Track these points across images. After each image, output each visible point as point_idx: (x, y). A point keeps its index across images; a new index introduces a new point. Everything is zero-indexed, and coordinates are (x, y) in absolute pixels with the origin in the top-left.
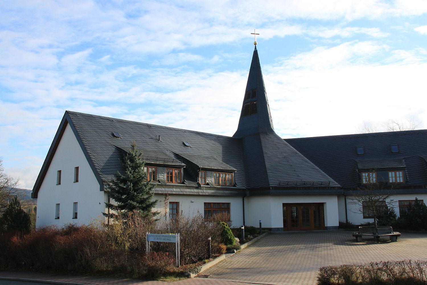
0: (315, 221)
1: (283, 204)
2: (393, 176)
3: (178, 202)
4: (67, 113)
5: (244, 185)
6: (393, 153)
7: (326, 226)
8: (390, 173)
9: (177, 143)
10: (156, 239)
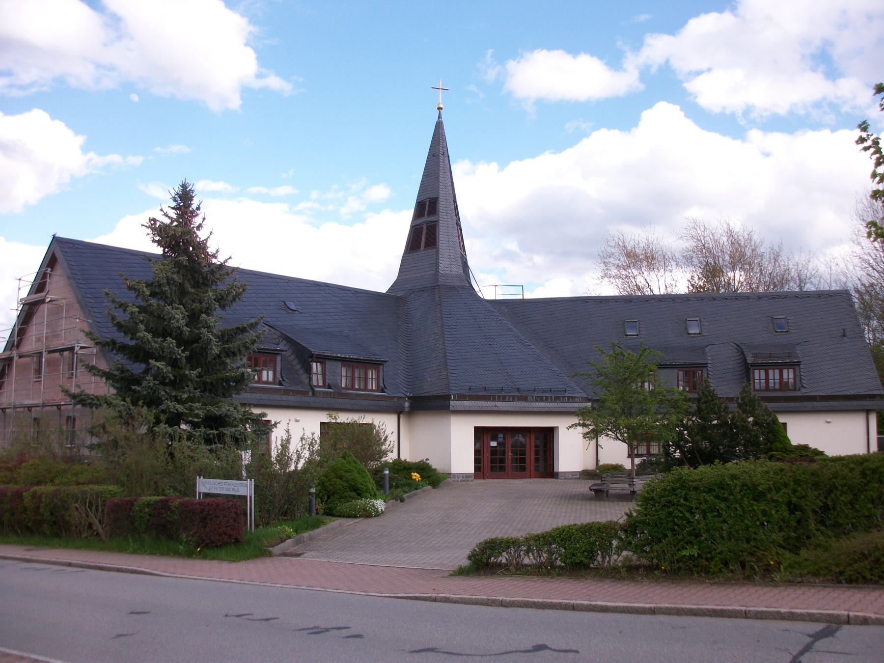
0: (537, 460)
1: (475, 428)
2: (761, 378)
3: (786, 423)
4: (57, 242)
5: (400, 389)
6: (692, 334)
7: (555, 471)
8: (756, 372)
9: (272, 304)
10: (213, 488)
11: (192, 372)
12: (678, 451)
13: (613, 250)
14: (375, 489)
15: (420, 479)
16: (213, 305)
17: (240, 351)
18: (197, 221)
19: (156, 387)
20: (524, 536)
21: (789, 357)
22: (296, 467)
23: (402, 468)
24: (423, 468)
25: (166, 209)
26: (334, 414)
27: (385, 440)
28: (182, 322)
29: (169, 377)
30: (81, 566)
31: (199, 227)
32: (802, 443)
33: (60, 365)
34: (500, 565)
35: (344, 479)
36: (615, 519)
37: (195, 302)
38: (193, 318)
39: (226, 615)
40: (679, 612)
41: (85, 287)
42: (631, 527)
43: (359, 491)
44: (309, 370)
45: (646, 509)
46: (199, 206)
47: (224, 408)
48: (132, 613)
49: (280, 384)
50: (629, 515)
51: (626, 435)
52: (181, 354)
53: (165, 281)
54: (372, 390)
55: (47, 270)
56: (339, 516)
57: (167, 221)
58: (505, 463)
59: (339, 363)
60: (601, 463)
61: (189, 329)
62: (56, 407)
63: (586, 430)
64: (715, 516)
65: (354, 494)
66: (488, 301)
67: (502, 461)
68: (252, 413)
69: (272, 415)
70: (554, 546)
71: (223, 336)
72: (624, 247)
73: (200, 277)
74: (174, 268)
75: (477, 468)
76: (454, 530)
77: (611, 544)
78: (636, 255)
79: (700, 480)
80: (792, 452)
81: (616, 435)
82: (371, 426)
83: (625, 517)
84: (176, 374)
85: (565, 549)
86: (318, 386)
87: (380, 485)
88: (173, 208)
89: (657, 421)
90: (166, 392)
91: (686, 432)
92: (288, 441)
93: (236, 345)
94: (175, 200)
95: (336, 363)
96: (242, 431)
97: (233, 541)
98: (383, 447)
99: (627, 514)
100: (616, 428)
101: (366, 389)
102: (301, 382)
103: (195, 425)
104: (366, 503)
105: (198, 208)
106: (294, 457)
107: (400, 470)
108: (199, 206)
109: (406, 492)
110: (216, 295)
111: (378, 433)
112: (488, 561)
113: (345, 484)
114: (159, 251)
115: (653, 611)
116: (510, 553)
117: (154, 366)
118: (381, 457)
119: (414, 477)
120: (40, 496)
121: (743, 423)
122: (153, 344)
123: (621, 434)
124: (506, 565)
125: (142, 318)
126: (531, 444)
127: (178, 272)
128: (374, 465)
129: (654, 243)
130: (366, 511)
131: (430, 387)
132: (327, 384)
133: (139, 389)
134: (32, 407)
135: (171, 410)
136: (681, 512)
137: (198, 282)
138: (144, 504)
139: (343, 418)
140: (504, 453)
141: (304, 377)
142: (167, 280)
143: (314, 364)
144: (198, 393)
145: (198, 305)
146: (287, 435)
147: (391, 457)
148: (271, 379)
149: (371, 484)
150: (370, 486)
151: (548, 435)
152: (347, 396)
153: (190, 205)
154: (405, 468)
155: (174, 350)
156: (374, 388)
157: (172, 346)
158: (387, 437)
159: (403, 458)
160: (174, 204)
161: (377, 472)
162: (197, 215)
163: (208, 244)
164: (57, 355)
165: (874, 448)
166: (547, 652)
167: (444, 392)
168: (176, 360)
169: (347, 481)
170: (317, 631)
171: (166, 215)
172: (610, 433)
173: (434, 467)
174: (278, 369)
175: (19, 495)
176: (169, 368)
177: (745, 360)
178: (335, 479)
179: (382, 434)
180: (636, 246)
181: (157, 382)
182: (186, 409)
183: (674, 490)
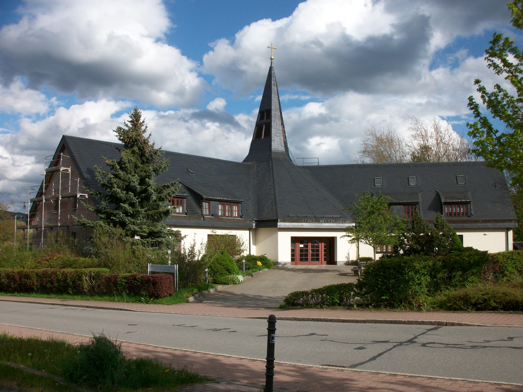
11: (142, 209)
12: (402, 250)
13: (369, 137)
14: (238, 270)
15: (261, 265)
16: (152, 174)
17: (166, 197)
18: (143, 128)
19: (124, 218)
20: (310, 290)
21: (465, 199)
22: (198, 258)
23: (251, 259)
24: (263, 259)
25: (127, 123)
26: (214, 230)
27: (243, 244)
28: (136, 183)
29: (130, 212)
30: (94, 308)
31: (144, 131)
32: (469, 246)
33: (68, 204)
34: (299, 305)
35: (222, 264)
36: (352, 282)
37: (142, 172)
38: (142, 181)
39: (173, 325)
40: (376, 322)
41: (81, 163)
42: (360, 285)
43: (230, 271)
44: (201, 207)
45: (366, 277)
46: (144, 121)
47: (158, 227)
48: (129, 325)
49: (186, 214)
50: (359, 280)
51: (371, 241)
52: (136, 200)
53: (127, 161)
54: (235, 217)
55: (61, 154)
56: (220, 284)
57: (127, 129)
58: (308, 257)
59: (218, 202)
60: (360, 257)
61: (140, 187)
62: (66, 227)
63: (350, 239)
64: (397, 281)
65: (227, 272)
66: (299, 167)
67: (306, 255)
68: (173, 230)
69: (184, 231)
70: (324, 295)
71: (157, 190)
72: (375, 135)
73: (145, 158)
74: (132, 154)
75: (293, 260)
76: (279, 290)
77: (350, 294)
78: (382, 140)
79: (390, 264)
80: (463, 251)
81: (366, 241)
82: (234, 236)
83: (357, 281)
84: (134, 211)
85: (329, 296)
86: (206, 215)
87: (241, 268)
88: (130, 122)
89: (388, 234)
90: (129, 220)
91: (406, 240)
92: (194, 245)
93: (164, 195)
94: (131, 118)
95: (216, 202)
96: (168, 240)
97: (169, 295)
98: (242, 248)
99: (358, 280)
100: (366, 237)
101: (232, 216)
102: (197, 213)
103: (142, 237)
104: (233, 277)
105: (143, 122)
106: (198, 253)
107: (251, 260)
108: (144, 121)
109: (254, 272)
110: (154, 169)
111: (239, 240)
112: (293, 302)
113: (222, 267)
114: (120, 142)
115: (364, 322)
116: (304, 298)
117: (123, 207)
118: (240, 253)
119: (258, 264)
120: (67, 274)
121: (436, 235)
122: (121, 194)
123: (369, 241)
124: (302, 304)
125: (115, 181)
126: (322, 246)
127: (133, 156)
128: (237, 257)
129: (392, 132)
130: (234, 281)
131: (266, 215)
132: (211, 214)
133: (115, 218)
134: (52, 227)
135: (132, 229)
136: (381, 279)
137: (144, 161)
138: (122, 277)
139: (220, 232)
140: (307, 251)
141: (199, 211)
142: (128, 160)
143: (204, 203)
144: (145, 220)
145: (144, 173)
146: (194, 242)
147: (246, 253)
148: (181, 211)
149: (236, 267)
150: (235, 268)
151: (331, 243)
152: (222, 219)
153: (139, 120)
154: (253, 259)
155: (132, 198)
156: (236, 216)
157: (131, 196)
158: (244, 242)
159: (252, 254)
160: (130, 119)
161: (238, 261)
162: (143, 125)
163: (149, 140)
164: (66, 199)
165: (511, 248)
166: (315, 336)
167: (275, 218)
168: (134, 203)
169: (224, 266)
170: (216, 330)
171: (127, 125)
172: (363, 240)
173: (269, 258)
174: (185, 206)
175: (54, 273)
176: (131, 208)
177: (440, 200)
178: (217, 265)
179: (241, 241)
180: (382, 134)
181: (124, 215)
182: (139, 228)
183: (379, 268)
